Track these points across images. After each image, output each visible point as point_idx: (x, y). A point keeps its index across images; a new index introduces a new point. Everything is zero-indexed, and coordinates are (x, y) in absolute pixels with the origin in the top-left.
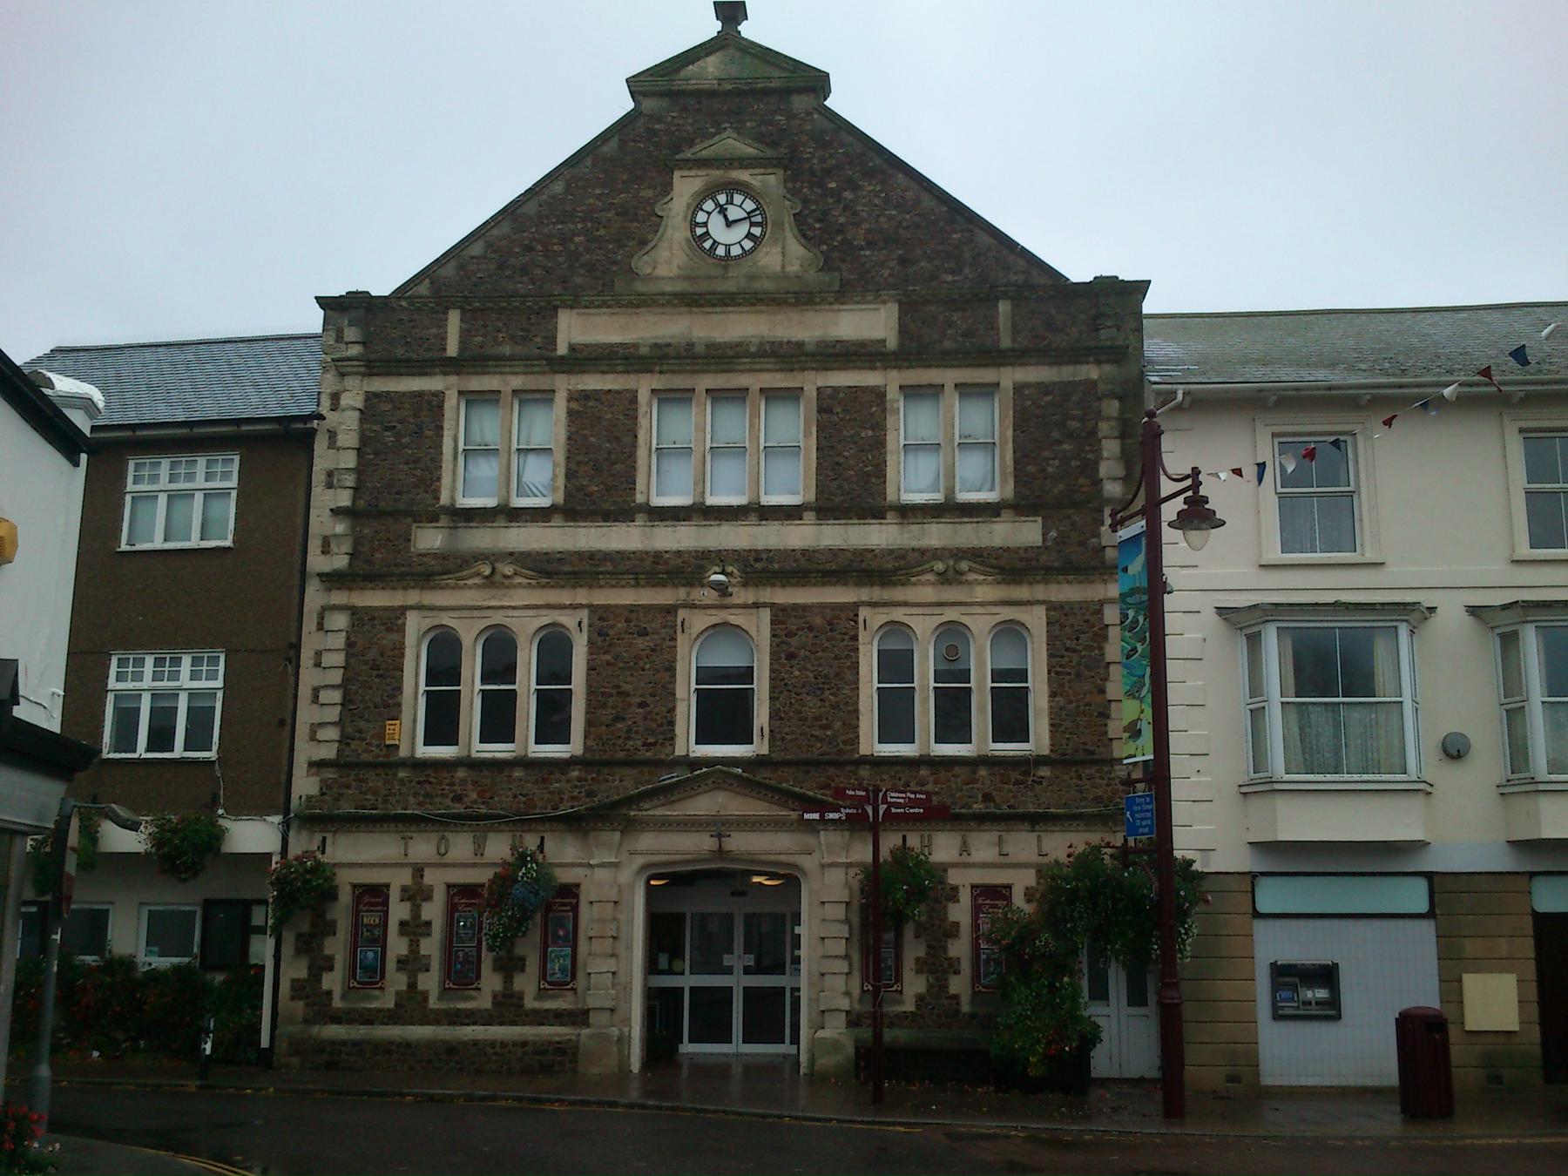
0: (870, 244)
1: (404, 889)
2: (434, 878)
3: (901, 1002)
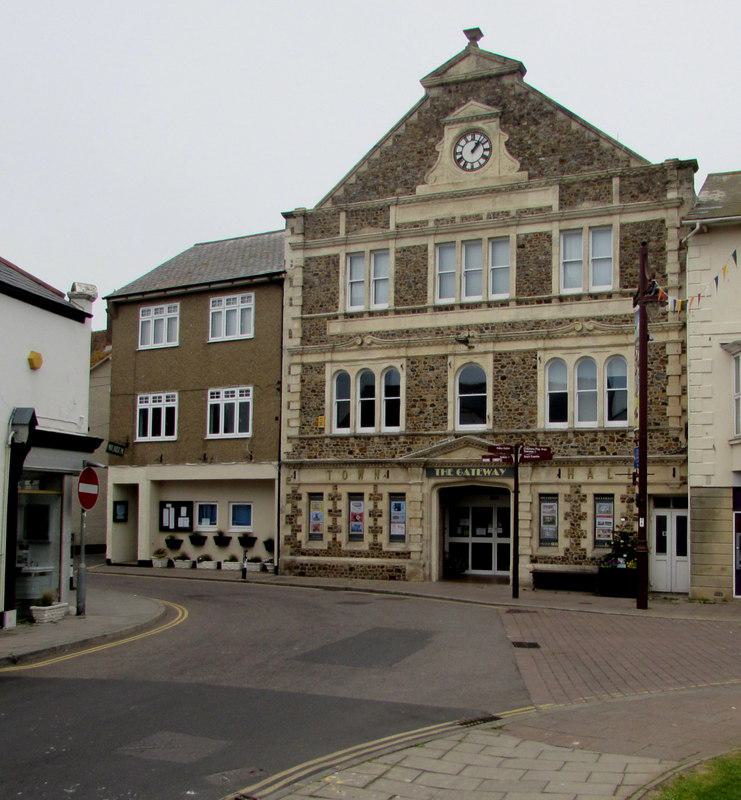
0: (544, 154)
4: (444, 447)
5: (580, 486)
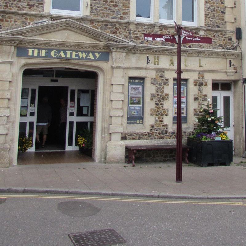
4: (44, 27)
5: (164, 72)
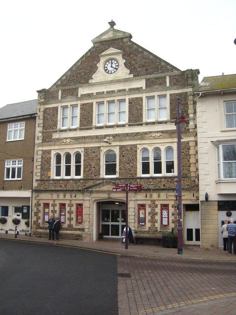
1: (52, 204)
2: (57, 202)
3: (169, 229)
